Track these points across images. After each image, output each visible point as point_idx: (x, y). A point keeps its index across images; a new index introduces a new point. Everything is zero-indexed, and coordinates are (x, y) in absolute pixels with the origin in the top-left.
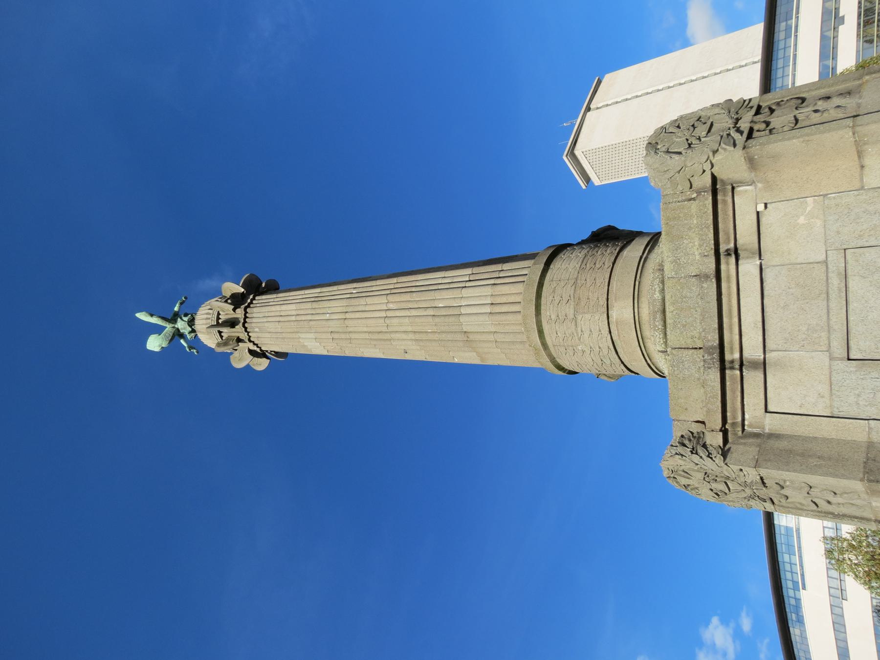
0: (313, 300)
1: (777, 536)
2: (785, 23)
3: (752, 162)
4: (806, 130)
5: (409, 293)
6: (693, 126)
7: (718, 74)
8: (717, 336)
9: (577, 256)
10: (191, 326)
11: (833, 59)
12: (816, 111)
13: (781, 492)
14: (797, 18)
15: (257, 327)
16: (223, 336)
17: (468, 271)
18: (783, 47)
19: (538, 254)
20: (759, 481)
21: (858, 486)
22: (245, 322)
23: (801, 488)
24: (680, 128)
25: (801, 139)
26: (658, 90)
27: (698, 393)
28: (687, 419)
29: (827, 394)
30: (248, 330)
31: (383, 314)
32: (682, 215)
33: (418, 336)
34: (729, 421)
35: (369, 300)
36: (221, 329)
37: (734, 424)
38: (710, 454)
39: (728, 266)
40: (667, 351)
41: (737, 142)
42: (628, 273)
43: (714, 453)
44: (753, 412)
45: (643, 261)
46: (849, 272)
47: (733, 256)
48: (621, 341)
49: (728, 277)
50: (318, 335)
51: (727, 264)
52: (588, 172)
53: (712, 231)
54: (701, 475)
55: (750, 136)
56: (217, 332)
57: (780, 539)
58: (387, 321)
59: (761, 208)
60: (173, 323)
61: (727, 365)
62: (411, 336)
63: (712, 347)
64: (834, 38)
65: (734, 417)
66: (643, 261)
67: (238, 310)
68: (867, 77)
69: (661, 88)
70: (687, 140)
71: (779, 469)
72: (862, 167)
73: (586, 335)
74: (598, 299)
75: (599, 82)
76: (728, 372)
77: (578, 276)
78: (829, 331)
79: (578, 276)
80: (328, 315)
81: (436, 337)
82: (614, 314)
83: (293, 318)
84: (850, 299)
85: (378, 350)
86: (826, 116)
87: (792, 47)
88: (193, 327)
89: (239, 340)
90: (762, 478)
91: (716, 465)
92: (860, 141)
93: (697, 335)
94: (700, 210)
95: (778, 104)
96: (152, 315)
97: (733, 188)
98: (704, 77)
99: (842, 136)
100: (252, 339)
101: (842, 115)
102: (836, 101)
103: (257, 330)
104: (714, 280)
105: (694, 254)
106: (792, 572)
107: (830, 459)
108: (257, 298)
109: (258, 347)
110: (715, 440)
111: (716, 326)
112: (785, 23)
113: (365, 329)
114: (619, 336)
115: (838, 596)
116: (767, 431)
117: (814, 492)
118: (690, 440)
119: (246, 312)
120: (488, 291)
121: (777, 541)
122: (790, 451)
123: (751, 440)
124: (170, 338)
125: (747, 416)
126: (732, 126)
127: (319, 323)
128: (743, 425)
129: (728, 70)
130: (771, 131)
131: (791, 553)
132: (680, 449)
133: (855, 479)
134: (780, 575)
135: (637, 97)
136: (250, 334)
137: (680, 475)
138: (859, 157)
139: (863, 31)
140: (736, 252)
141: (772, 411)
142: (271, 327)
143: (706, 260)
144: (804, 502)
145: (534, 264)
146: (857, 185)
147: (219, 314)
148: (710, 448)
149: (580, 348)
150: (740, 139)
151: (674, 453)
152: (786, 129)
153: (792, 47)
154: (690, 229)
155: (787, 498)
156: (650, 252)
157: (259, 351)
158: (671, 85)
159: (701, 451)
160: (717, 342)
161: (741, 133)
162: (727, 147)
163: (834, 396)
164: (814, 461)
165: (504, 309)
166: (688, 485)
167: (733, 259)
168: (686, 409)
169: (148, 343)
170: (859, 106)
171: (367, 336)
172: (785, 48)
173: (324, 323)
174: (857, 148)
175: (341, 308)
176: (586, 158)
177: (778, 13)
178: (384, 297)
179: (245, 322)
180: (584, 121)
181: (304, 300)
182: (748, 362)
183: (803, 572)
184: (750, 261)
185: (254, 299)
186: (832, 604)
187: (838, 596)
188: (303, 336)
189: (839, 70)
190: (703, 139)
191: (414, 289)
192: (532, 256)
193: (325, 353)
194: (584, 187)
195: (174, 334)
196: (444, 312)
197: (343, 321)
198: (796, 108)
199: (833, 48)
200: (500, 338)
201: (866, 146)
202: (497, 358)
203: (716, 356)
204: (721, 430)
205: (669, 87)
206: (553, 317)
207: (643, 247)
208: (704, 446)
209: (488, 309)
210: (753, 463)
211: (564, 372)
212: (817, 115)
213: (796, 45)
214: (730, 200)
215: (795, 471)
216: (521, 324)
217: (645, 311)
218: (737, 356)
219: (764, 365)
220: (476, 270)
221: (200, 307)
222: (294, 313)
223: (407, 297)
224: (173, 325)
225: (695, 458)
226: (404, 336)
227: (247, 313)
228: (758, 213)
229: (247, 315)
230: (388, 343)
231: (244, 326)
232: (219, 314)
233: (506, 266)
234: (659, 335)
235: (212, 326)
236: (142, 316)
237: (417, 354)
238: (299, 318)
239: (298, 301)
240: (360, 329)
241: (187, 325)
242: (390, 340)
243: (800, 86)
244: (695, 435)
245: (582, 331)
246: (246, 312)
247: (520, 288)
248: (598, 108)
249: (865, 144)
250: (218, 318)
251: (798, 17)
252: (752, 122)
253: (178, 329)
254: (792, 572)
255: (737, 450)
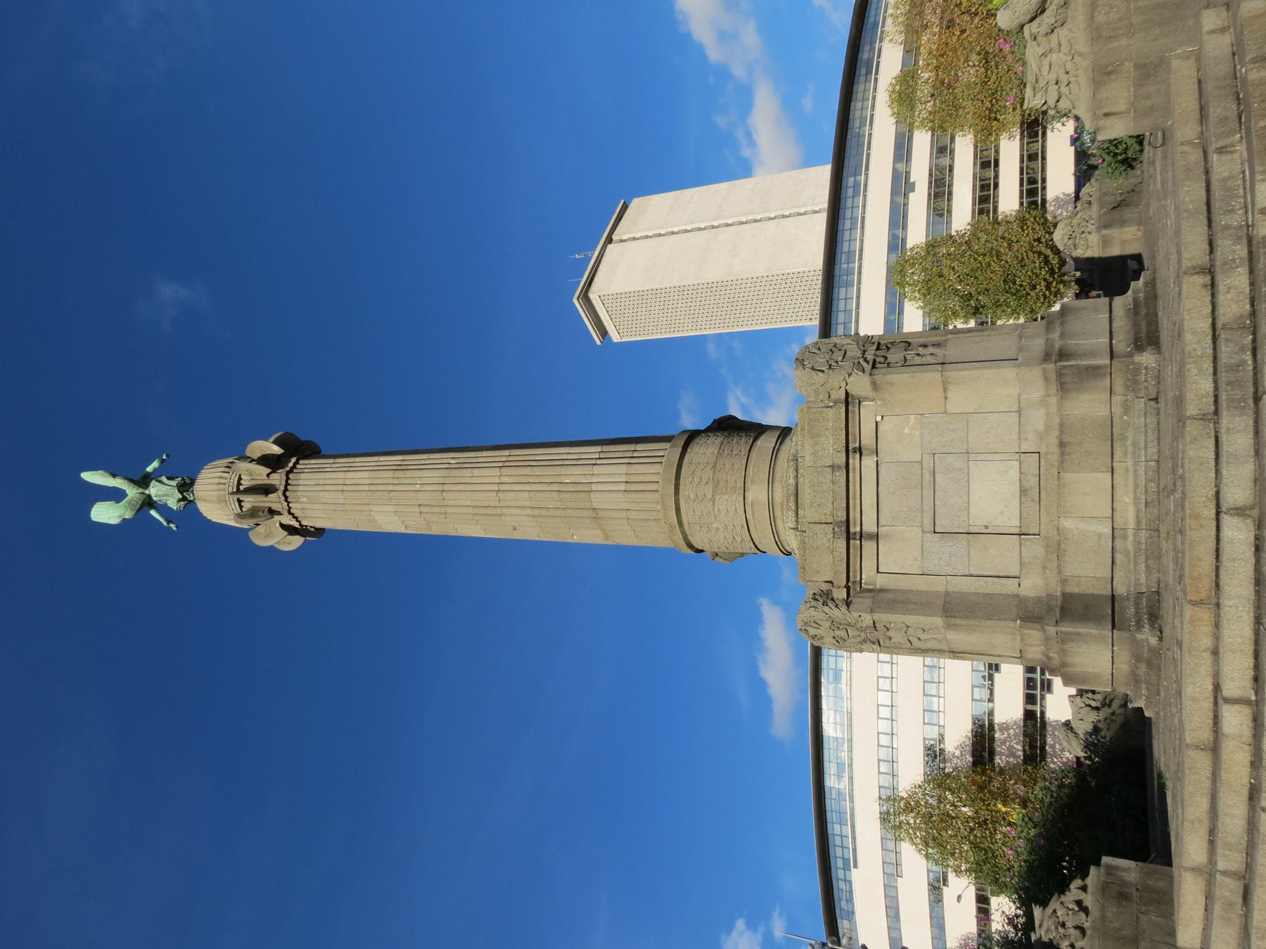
0: (394, 468)
1: (828, 801)
2: (853, 178)
3: (875, 386)
4: (912, 368)
5: (529, 468)
6: (831, 350)
7: (772, 219)
8: (845, 514)
9: (714, 443)
10: (181, 493)
11: (903, 228)
12: (918, 355)
13: (887, 634)
14: (867, 175)
15: (304, 496)
16: (242, 507)
17: (598, 449)
18: (851, 206)
19: (674, 436)
20: (872, 625)
21: (938, 621)
22: (286, 490)
23: (900, 630)
24: (820, 350)
25: (909, 375)
26: (700, 229)
27: (828, 559)
28: (819, 580)
29: (920, 558)
30: (289, 500)
31: (496, 487)
32: (820, 418)
33: (536, 512)
34: (851, 580)
35: (476, 472)
36: (242, 497)
37: (854, 582)
38: (837, 605)
39: (854, 460)
40: (797, 528)
41: (865, 369)
42: (764, 461)
43: (840, 604)
44: (868, 574)
45: (776, 452)
46: (936, 470)
47: (858, 453)
48: (754, 520)
49: (854, 469)
50: (400, 509)
51: (854, 458)
52: (605, 324)
53: (844, 433)
54: (827, 624)
55: (874, 367)
56: (236, 500)
57: (830, 804)
58: (501, 495)
59: (879, 419)
60: (143, 488)
61: (851, 536)
62: (529, 512)
63: (841, 522)
64: (904, 205)
65: (855, 577)
66: (776, 452)
67: (274, 476)
68: (950, 336)
69: (703, 226)
70: (828, 362)
71: (887, 613)
72: (946, 398)
73: (722, 514)
74: (736, 482)
75: (625, 207)
76: (851, 541)
77: (716, 461)
78: (922, 512)
79: (716, 461)
80: (418, 486)
81: (558, 513)
82: (750, 496)
83: (366, 488)
84: (936, 490)
85: (479, 526)
86: (924, 360)
87: (860, 207)
88: (185, 494)
89: (272, 512)
90: (874, 622)
91: (839, 614)
93: (829, 513)
94: (836, 416)
95: (892, 343)
96: (114, 476)
97: (860, 402)
98: (756, 221)
99: (932, 377)
100: (292, 511)
102: (931, 350)
103: (304, 499)
104: (844, 470)
105: (828, 449)
106: (842, 847)
107: (921, 604)
108: (301, 462)
109: (297, 521)
110: (840, 594)
111: (845, 505)
112: (853, 178)
113: (469, 503)
114: (753, 516)
115: (892, 870)
116: (878, 587)
117: (910, 631)
118: (821, 596)
119: (288, 478)
120: (623, 469)
121: (827, 809)
122: (895, 601)
123: (867, 594)
124: (138, 507)
125: (863, 576)
126: (861, 356)
127: (406, 494)
128: (861, 584)
129: (784, 216)
130: (888, 364)
131: (842, 823)
132: (814, 603)
133: (937, 616)
134: (829, 850)
135: (673, 233)
136: (290, 505)
137: (811, 626)
138: (945, 391)
139: (934, 203)
140: (860, 450)
141: (882, 571)
142: (328, 497)
143: (839, 454)
144: (902, 642)
145: (672, 446)
146: (943, 411)
147: (240, 479)
148: (837, 602)
149: (714, 525)
150: (867, 367)
151: (808, 606)
152: (898, 365)
153: (860, 207)
154: (827, 429)
155: (890, 639)
156: (781, 444)
157: (298, 527)
158: (716, 224)
159: (830, 603)
160: (845, 518)
161: (868, 362)
162: (859, 373)
163: (924, 560)
164: (911, 607)
165: (641, 487)
166: (816, 635)
167: (858, 455)
168: (818, 572)
169: (93, 509)
170: (945, 356)
171: (470, 510)
172: (852, 207)
173: (413, 494)
175: (438, 479)
176: (604, 304)
177: (846, 165)
178: (498, 469)
179: (286, 490)
180: (603, 255)
181: (381, 468)
182: (867, 534)
183: (855, 846)
184: (869, 457)
185: (297, 463)
186: (886, 883)
187: (892, 870)
188: (373, 508)
189: (909, 245)
190: (840, 363)
191: (533, 463)
192: (668, 439)
193: (402, 530)
194: (598, 343)
195: (143, 502)
196: (571, 488)
197: (439, 493)
198: (905, 350)
199: (903, 217)
200: (632, 515)
202: (626, 537)
203: (843, 529)
204: (845, 587)
205: (713, 227)
206: (692, 496)
207: (775, 439)
208: (832, 599)
209: (623, 487)
210: (869, 610)
211: (692, 550)
212: (919, 358)
213: (864, 206)
214: (857, 411)
215: (898, 614)
216: (658, 502)
217: (779, 494)
218: (858, 529)
219: (876, 537)
220: (606, 448)
221: (202, 469)
222: (367, 482)
223: (527, 471)
224: (143, 490)
225: (826, 609)
226: (519, 511)
227: (289, 479)
228: (877, 422)
229: (289, 482)
230: (498, 518)
231: (284, 494)
232: (240, 479)
233: (640, 447)
234: (791, 515)
235: (233, 493)
236: (88, 476)
237: (529, 531)
238: (372, 488)
239: (371, 468)
240: (462, 503)
241: (176, 491)
242: (500, 515)
243: (907, 333)
244: (825, 592)
245: (719, 510)
246: (288, 478)
247: (658, 468)
248: (622, 241)
250: (239, 484)
251: (867, 174)
252: (875, 355)
253: (149, 497)
254: (842, 847)
255: (857, 602)
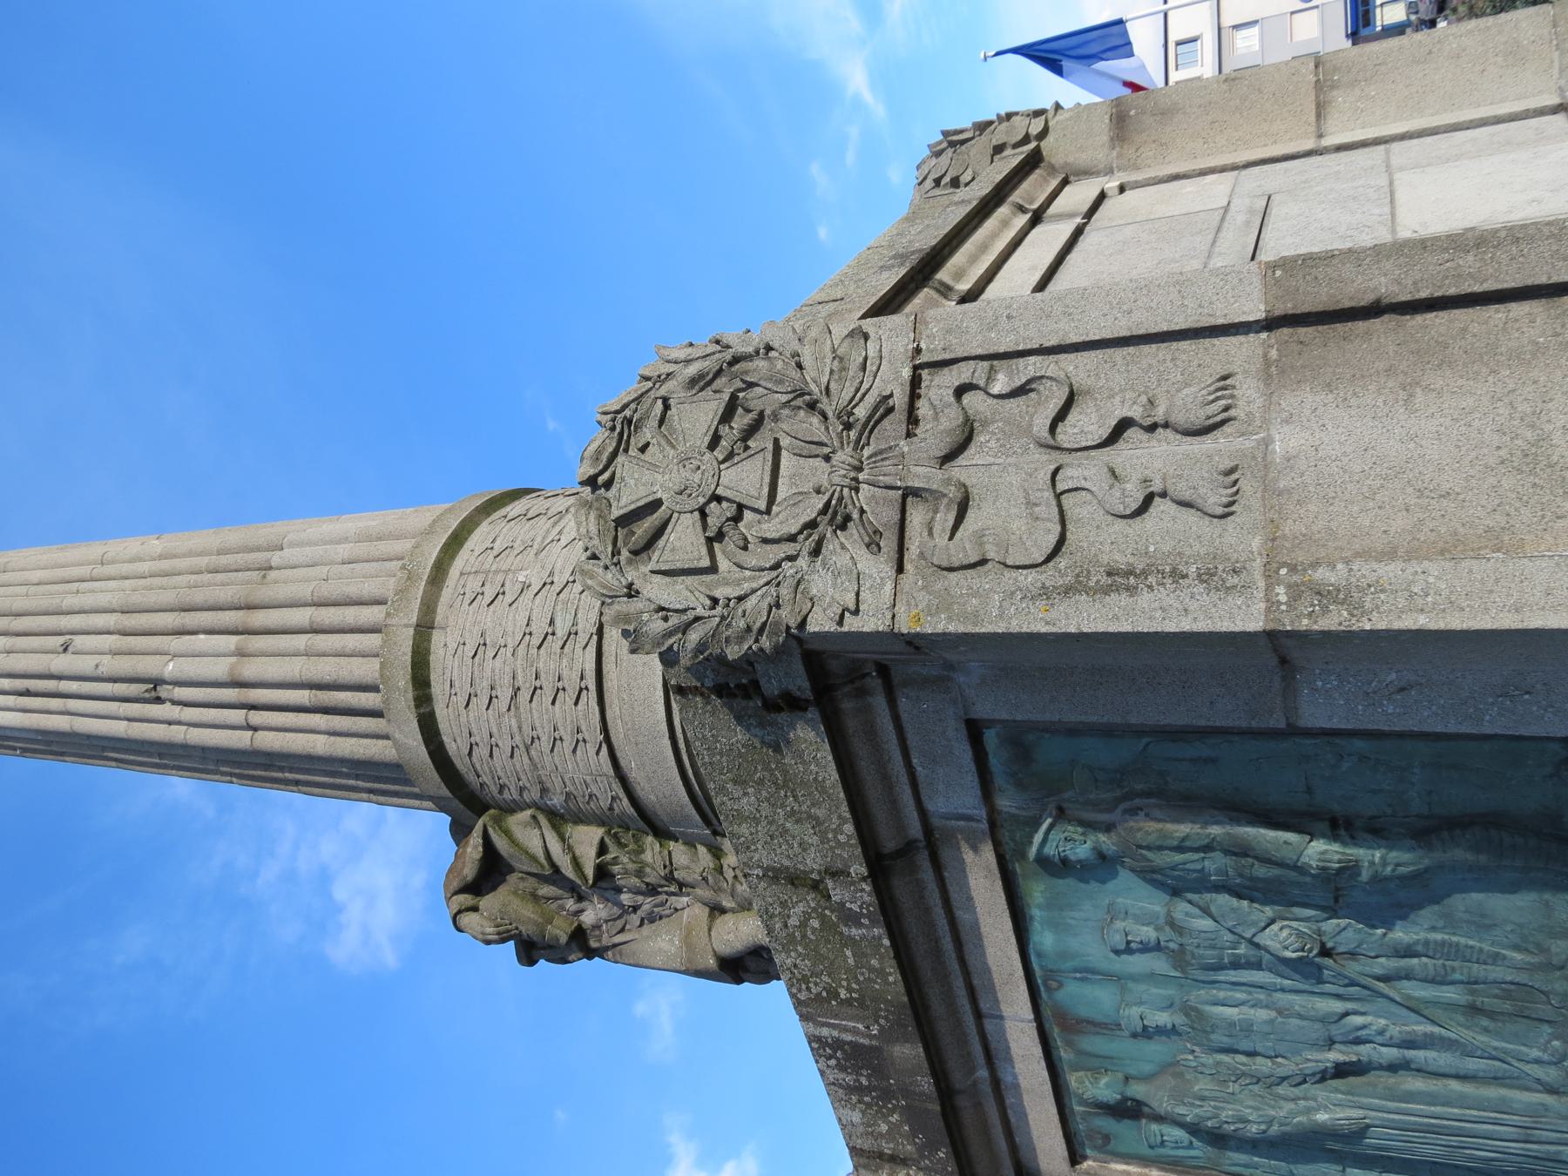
47: (1026, 218)
92: (1325, 81)
101: (1225, 1039)
138: (1318, 116)
174: (1317, 97)
201: (1335, 93)
249: (1333, 87)
